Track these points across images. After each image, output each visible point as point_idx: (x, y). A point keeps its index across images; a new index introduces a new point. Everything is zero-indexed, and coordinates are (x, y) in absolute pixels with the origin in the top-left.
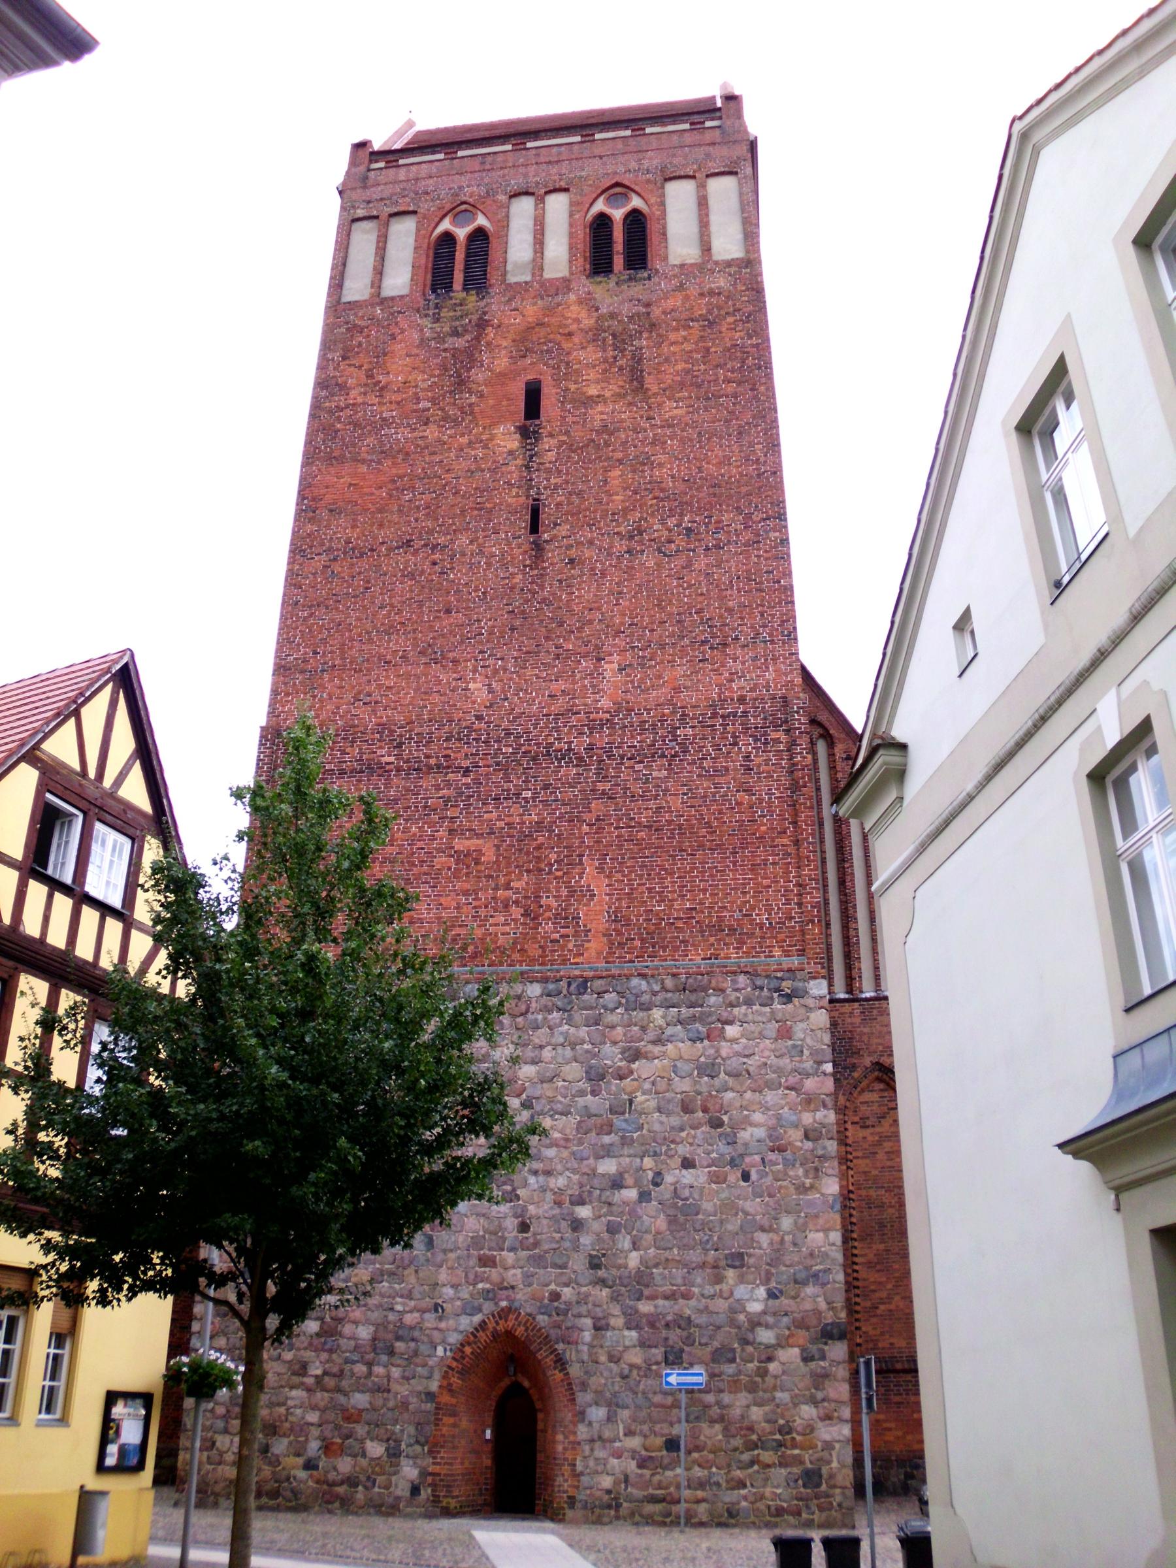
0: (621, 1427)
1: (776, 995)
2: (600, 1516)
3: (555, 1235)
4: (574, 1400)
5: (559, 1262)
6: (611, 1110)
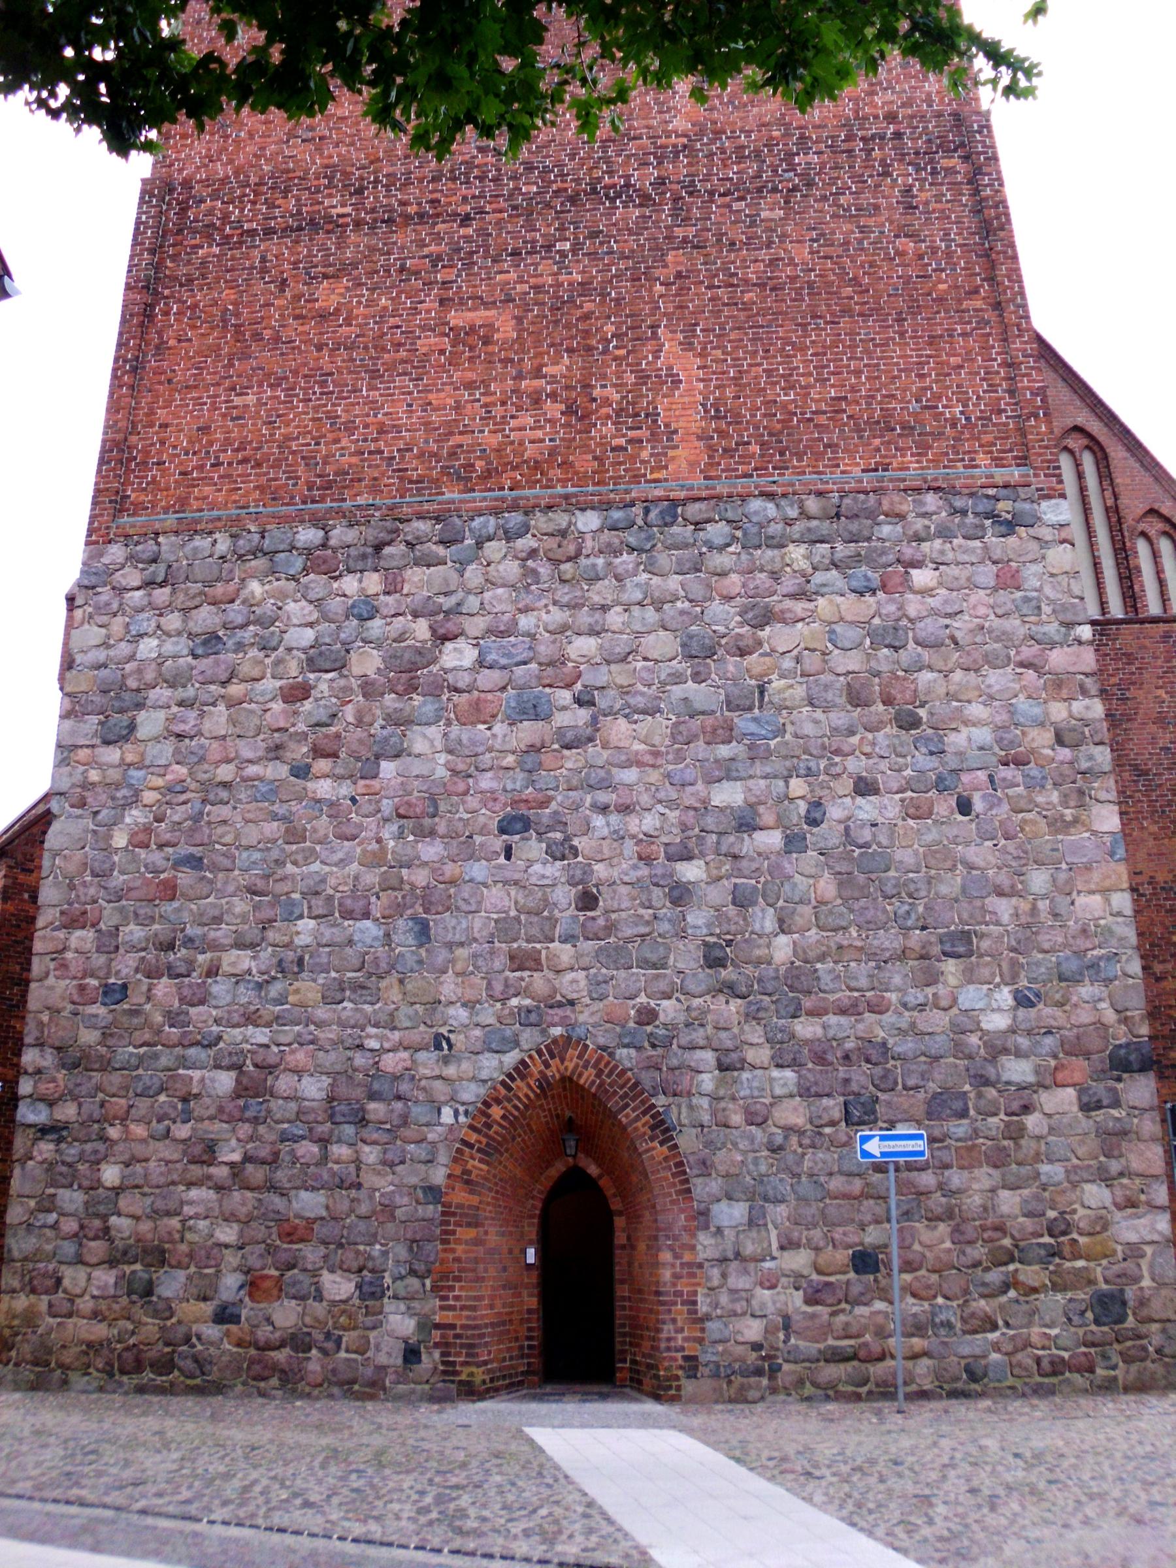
0: (774, 1234)
1: (988, 522)
2: (743, 1388)
3: (641, 911)
4: (689, 1191)
5: (653, 957)
6: (728, 703)
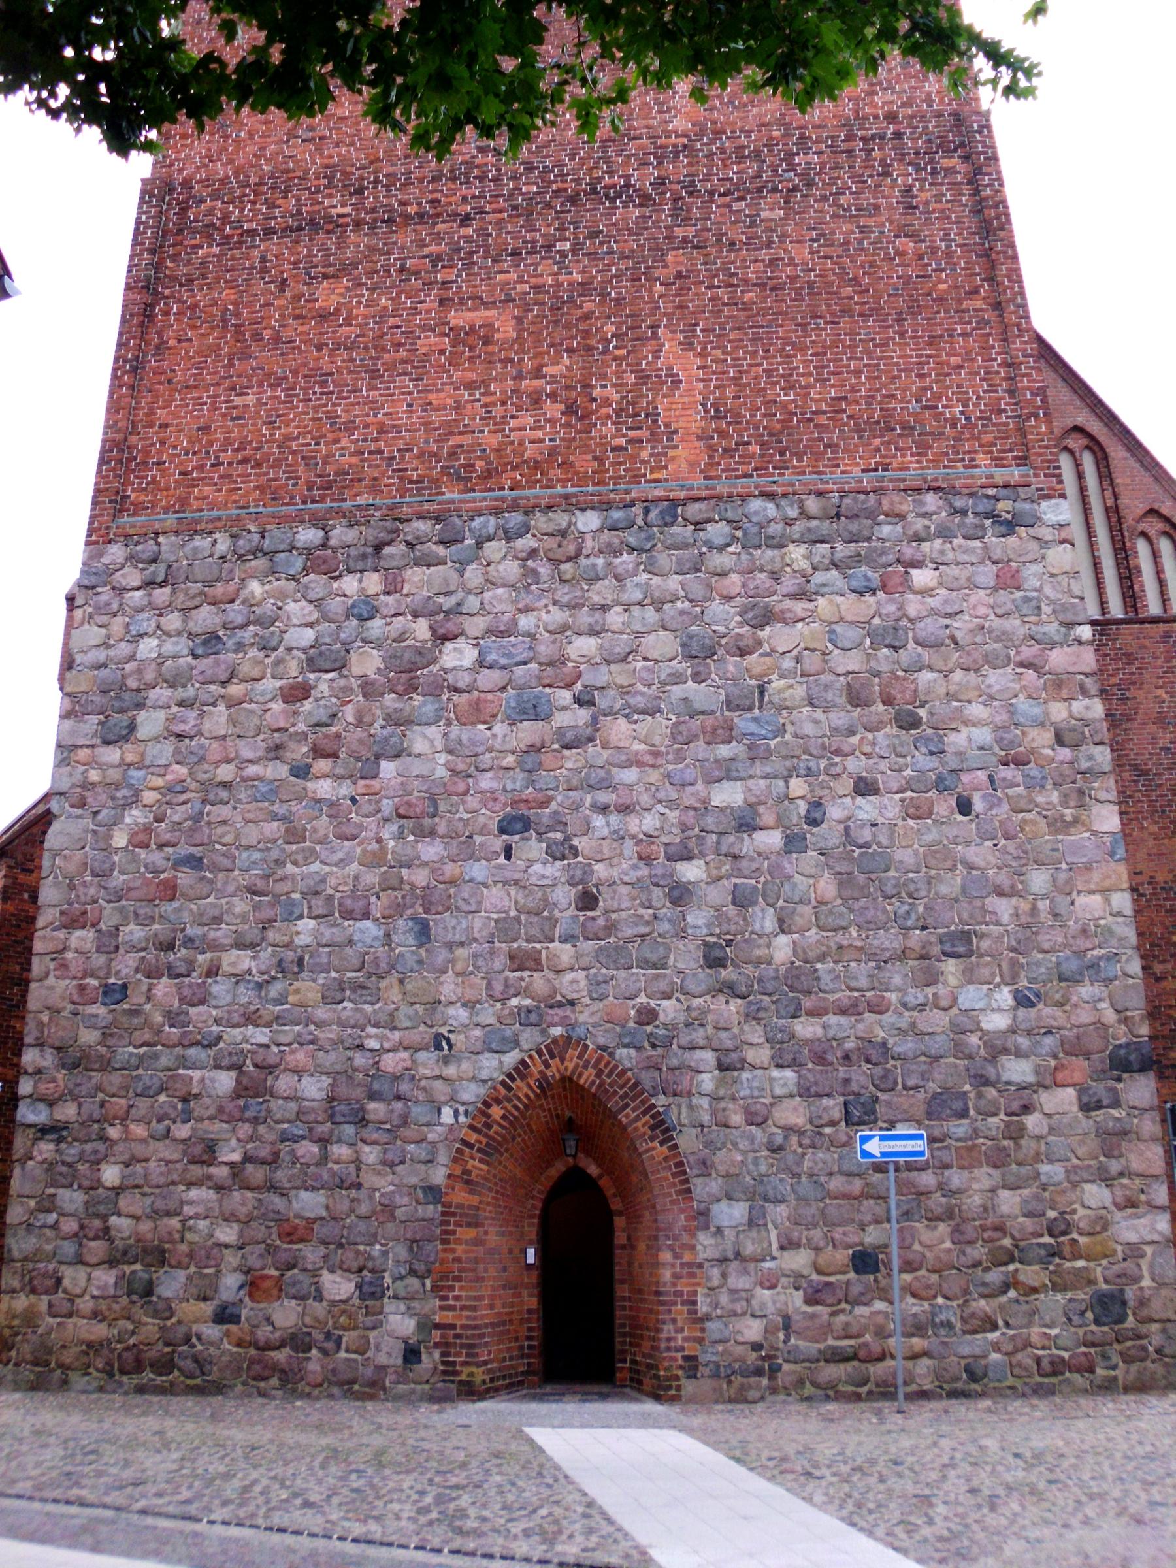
0: (774, 1234)
1: (988, 522)
2: (743, 1388)
3: (641, 911)
4: (689, 1191)
5: (653, 957)
6: (728, 703)
